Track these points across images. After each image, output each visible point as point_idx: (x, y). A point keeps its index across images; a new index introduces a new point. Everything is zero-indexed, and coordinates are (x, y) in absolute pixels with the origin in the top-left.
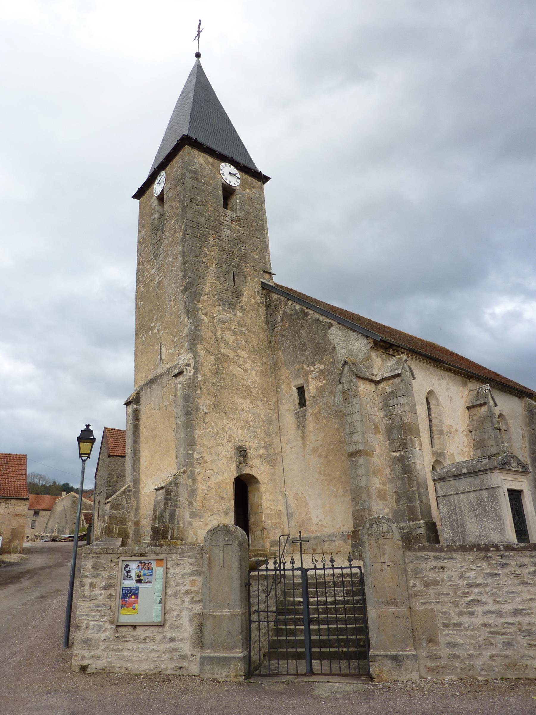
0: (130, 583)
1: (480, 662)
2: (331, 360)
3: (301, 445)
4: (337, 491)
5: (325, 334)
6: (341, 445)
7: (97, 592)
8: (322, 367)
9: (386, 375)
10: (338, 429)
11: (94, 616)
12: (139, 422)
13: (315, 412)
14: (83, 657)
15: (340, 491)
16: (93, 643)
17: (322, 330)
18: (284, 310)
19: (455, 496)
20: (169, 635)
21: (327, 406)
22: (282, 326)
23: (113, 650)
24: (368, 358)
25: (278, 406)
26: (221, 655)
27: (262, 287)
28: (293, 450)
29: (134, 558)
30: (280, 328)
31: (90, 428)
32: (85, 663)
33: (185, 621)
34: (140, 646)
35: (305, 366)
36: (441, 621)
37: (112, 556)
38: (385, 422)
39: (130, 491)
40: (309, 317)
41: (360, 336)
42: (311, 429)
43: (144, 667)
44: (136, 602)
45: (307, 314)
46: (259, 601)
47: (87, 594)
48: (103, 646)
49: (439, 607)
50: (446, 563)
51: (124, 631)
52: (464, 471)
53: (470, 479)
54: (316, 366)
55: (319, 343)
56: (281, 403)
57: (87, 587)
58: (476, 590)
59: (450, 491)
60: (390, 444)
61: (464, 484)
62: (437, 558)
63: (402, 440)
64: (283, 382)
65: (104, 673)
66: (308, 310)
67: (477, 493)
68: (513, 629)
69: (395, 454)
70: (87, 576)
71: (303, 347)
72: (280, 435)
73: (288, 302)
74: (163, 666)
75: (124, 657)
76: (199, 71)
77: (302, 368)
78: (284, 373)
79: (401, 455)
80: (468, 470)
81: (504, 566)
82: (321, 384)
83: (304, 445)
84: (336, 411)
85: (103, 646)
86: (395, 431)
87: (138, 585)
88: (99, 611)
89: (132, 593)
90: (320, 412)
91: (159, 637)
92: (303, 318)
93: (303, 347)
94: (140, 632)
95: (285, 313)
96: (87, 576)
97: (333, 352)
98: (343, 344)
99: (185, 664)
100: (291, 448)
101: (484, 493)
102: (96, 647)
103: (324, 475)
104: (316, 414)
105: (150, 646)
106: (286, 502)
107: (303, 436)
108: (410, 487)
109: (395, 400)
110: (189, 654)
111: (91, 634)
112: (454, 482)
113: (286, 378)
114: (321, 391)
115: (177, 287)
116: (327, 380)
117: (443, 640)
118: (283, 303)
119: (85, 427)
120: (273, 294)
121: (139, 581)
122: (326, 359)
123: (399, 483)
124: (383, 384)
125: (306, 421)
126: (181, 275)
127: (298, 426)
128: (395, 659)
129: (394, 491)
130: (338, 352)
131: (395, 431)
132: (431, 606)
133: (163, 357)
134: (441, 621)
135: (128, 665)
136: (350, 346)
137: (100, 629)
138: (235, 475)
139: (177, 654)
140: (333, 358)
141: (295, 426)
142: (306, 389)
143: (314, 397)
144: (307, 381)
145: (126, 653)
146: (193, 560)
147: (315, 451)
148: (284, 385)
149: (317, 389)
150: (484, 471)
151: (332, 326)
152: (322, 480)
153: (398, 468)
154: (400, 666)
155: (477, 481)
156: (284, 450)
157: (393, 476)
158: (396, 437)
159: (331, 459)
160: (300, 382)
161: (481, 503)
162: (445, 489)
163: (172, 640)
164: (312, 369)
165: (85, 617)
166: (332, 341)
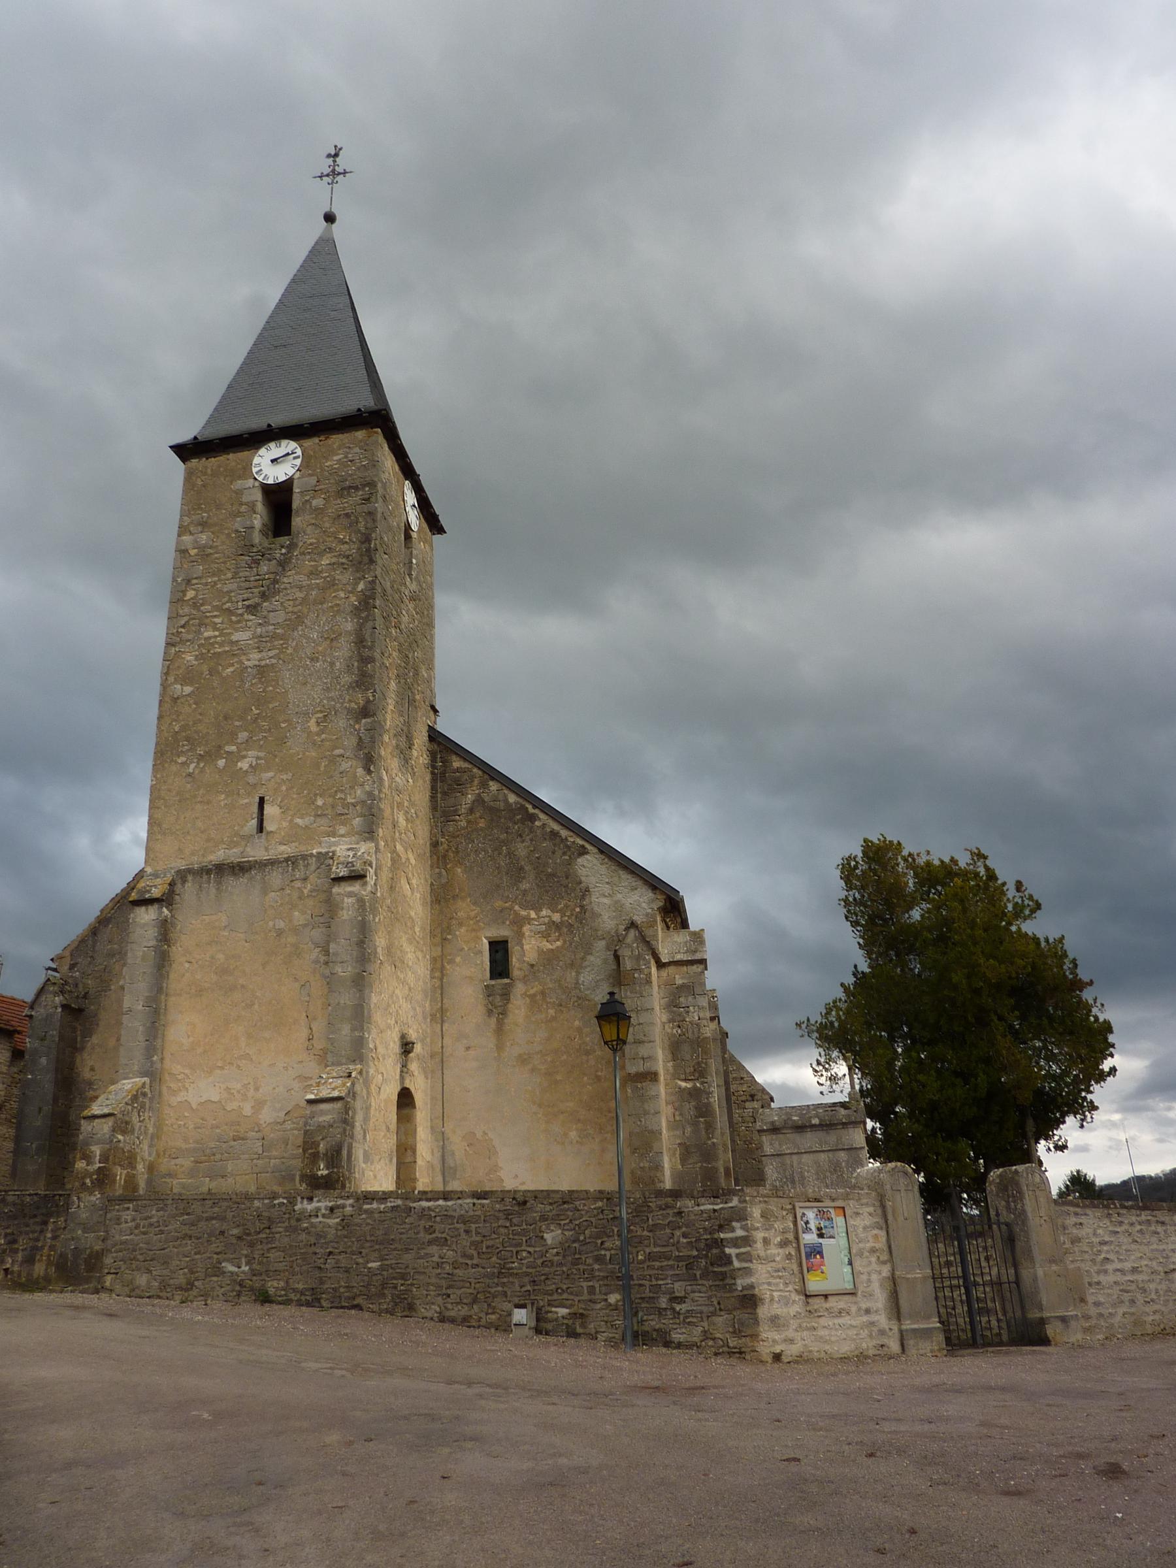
0: (810, 1238)
1: (1118, 1319)
2: (578, 910)
3: (492, 1045)
4: (566, 1135)
5: (569, 864)
6: (584, 1057)
7: (773, 1250)
8: (556, 917)
9: (678, 957)
10: (579, 1030)
11: (777, 1284)
12: (169, 946)
13: (532, 992)
14: (774, 1341)
15: (573, 1134)
16: (782, 1321)
17: (564, 854)
18: (479, 794)
19: (795, 1157)
20: (864, 1306)
21: (560, 985)
22: (469, 822)
23: (808, 1329)
24: (652, 924)
25: (443, 967)
26: (922, 1326)
27: (429, 736)
28: (471, 1052)
29: (808, 1204)
30: (463, 824)
31: (616, 996)
32: (777, 1349)
33: (876, 1287)
34: (837, 1321)
35: (517, 908)
36: (1086, 1280)
37: (782, 1200)
38: (669, 1031)
39: (144, 1095)
40: (537, 823)
41: (640, 883)
42: (521, 1021)
43: (846, 1349)
44: (822, 1264)
45: (532, 818)
46: (935, 1260)
47: (762, 1254)
48: (794, 1324)
49: (1083, 1265)
50: (1083, 1219)
51: (817, 1303)
52: (815, 1121)
53: (821, 1134)
54: (544, 913)
55: (553, 875)
56: (451, 962)
57: (759, 1245)
58: (1105, 1248)
59: (785, 1149)
60: (674, 1067)
61: (810, 1140)
62: (1076, 1214)
63: (698, 1063)
64: (461, 924)
65: (800, 1359)
66: (536, 811)
67: (830, 1155)
68: (1133, 1287)
69: (683, 1084)
70: (757, 1229)
71: (517, 873)
72: (443, 1021)
73: (491, 783)
74: (864, 1345)
75: (821, 1337)
76: (323, 261)
77: (511, 909)
78: (464, 908)
79: (695, 1087)
80: (821, 1120)
81: (1121, 1223)
82: (553, 947)
83: (500, 1047)
84: (579, 998)
85: (794, 1324)
86: (686, 1048)
87: (821, 1240)
88: (780, 1278)
89: (816, 1251)
90: (543, 993)
91: (854, 1309)
92: (522, 821)
93: (517, 873)
94: (833, 1302)
95: (479, 800)
96: (757, 1229)
97: (583, 897)
98: (607, 889)
99: (885, 1341)
100: (468, 1048)
101: (842, 1154)
102: (786, 1326)
103: (540, 1106)
104: (534, 995)
105: (845, 1320)
106: (443, 1148)
107: (500, 1030)
108: (709, 1139)
109: (690, 998)
110: (887, 1328)
111: (777, 1309)
112: (796, 1137)
113: (469, 918)
114: (549, 959)
115: (329, 699)
116: (565, 941)
117: (1091, 1299)
118: (476, 782)
119: (608, 997)
120: (454, 757)
121: (821, 1236)
122: (566, 906)
123: (689, 1130)
124: (671, 970)
125: (510, 1006)
126: (347, 679)
127: (490, 1013)
128: (1064, 1320)
129: (678, 1141)
130: (594, 899)
131: (686, 1048)
132: (1078, 1264)
133: (269, 826)
134: (1086, 1280)
135: (827, 1347)
136: (619, 896)
137: (787, 1302)
138: (399, 1089)
139: (875, 1329)
140: (582, 907)
141: (481, 1009)
142: (514, 949)
143: (532, 966)
144: (520, 935)
145: (821, 1333)
146: (871, 1209)
147: (523, 1060)
148: (463, 930)
149: (541, 952)
150: (845, 1125)
151: (587, 853)
152: (535, 1113)
153: (689, 1108)
154: (1068, 1327)
155: (832, 1138)
156: (448, 1051)
157: (677, 1118)
158: (688, 1057)
159: (559, 1078)
160: (501, 932)
161: (836, 1167)
162: (777, 1145)
163: (868, 1311)
164: (533, 915)
165: (766, 1286)
166: (583, 879)
